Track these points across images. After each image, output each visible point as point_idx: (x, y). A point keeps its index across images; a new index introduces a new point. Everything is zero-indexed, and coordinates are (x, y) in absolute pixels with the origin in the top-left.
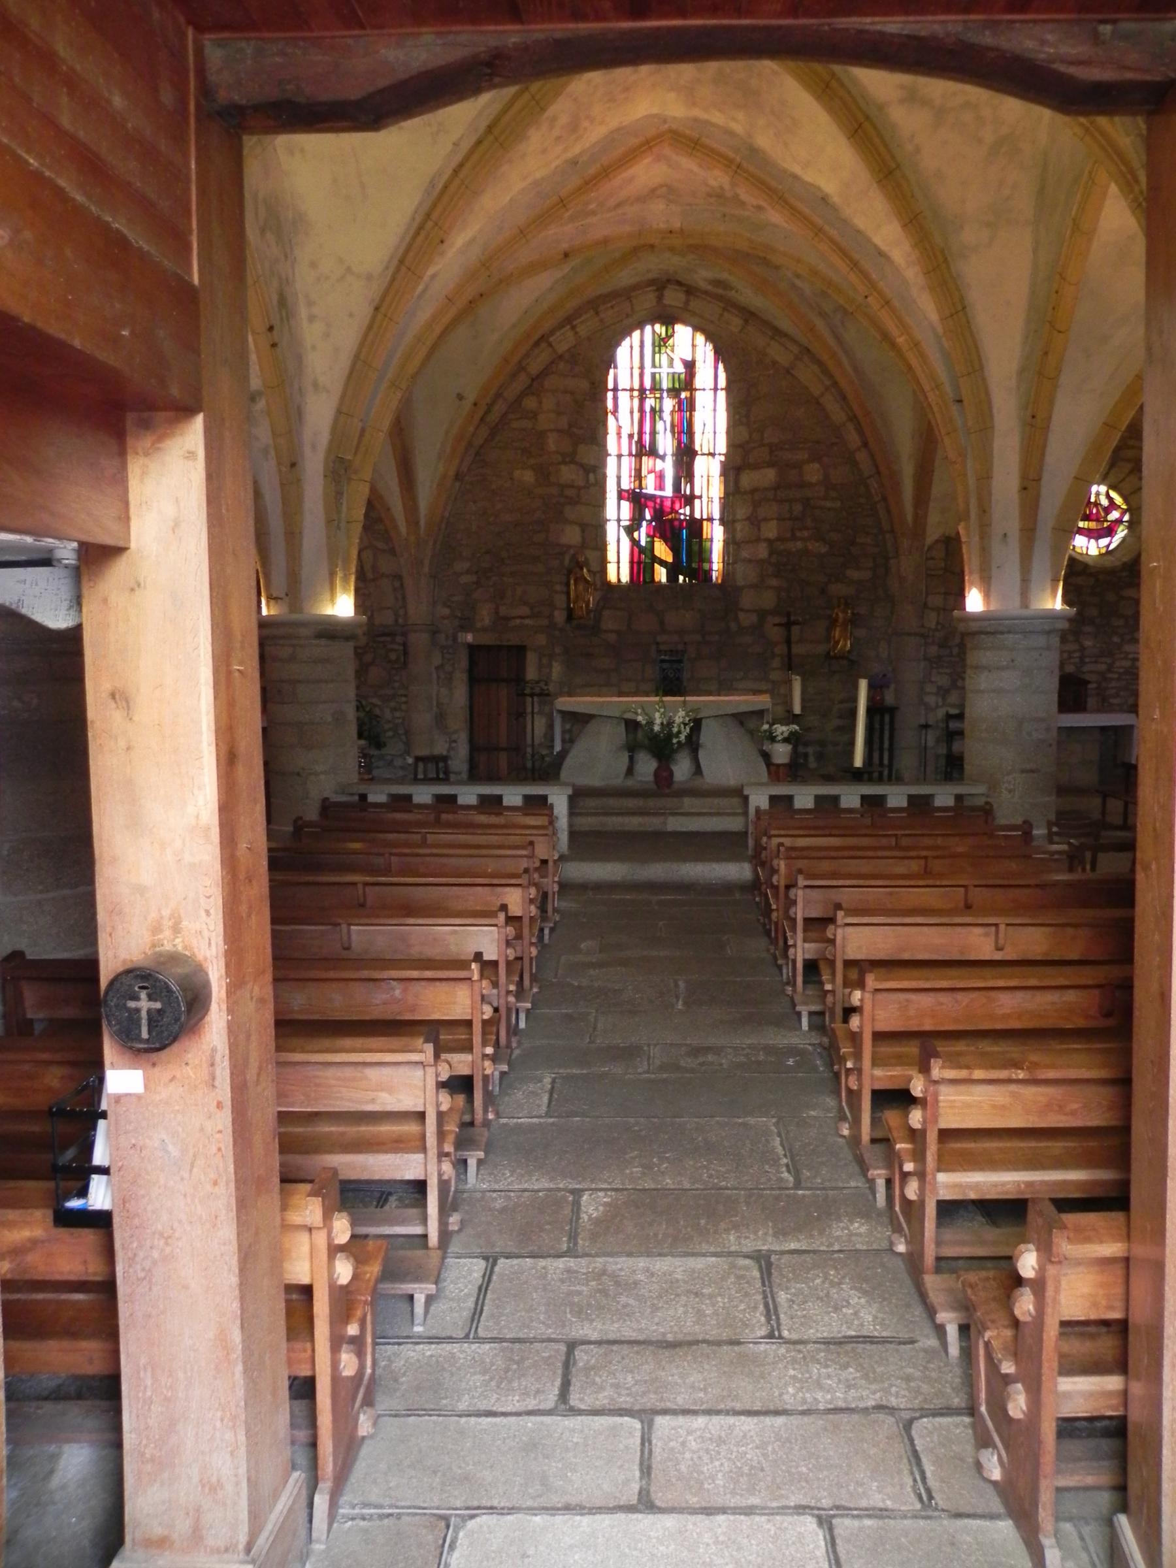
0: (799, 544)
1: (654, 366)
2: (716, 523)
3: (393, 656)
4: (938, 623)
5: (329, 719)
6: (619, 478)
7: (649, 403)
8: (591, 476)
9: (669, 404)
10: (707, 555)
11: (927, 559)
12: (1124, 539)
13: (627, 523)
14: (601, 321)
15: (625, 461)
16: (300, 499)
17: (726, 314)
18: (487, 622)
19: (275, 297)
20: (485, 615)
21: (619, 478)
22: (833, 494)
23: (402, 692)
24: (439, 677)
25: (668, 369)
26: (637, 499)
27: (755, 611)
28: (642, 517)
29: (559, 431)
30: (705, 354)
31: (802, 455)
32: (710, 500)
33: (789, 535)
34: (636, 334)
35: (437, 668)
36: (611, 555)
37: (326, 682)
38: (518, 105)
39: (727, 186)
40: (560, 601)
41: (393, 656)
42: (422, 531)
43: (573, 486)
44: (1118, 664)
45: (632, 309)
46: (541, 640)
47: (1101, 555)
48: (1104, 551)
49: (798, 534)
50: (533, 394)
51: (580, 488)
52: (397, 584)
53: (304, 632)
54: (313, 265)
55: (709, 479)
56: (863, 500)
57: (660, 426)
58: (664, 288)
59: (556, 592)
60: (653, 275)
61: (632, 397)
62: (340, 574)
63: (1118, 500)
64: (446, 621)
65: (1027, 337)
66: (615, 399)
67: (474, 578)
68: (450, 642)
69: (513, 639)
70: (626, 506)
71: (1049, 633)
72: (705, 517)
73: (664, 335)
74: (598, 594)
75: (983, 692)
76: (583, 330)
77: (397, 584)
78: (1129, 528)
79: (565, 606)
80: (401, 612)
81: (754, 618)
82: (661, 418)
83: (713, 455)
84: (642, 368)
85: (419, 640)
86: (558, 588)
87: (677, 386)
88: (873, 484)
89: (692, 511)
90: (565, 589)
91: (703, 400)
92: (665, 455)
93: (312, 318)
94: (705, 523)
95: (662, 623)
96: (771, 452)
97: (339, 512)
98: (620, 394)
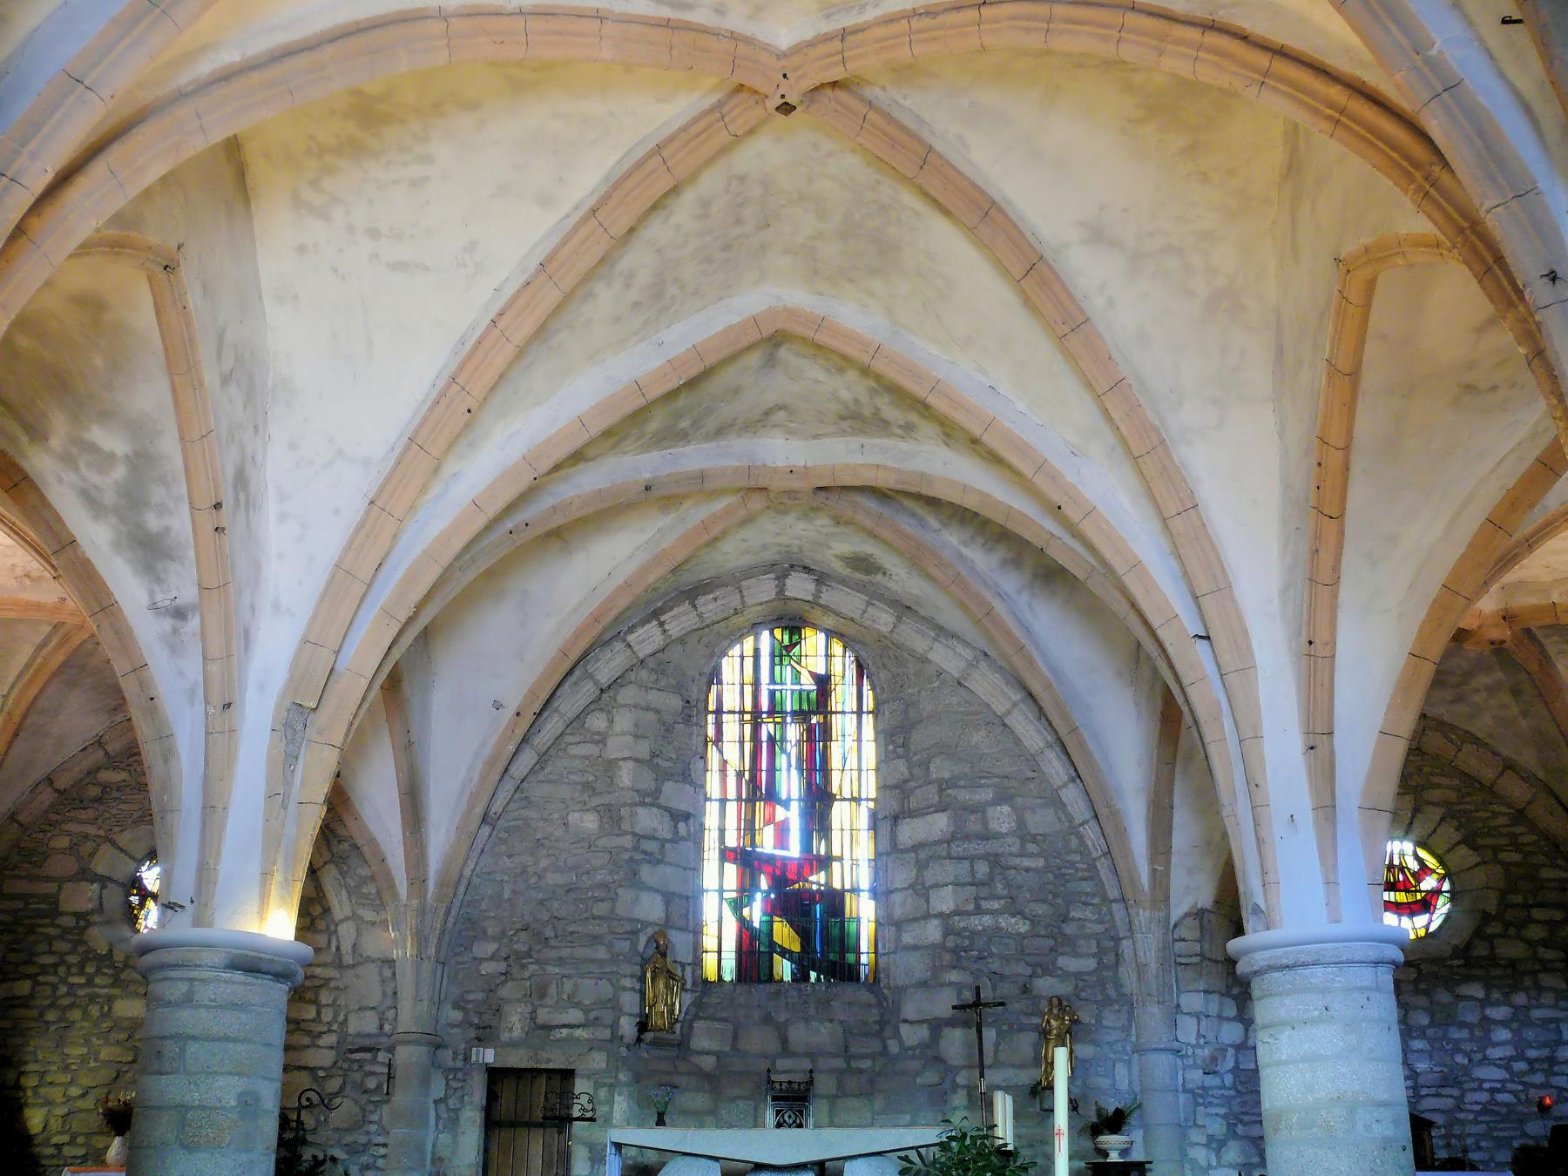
0: (987, 920)
1: (772, 681)
2: (865, 896)
3: (371, 1083)
4: (1199, 1035)
5: (233, 1103)
6: (722, 831)
7: (767, 729)
8: (682, 825)
9: (793, 732)
10: (853, 941)
11: (1175, 940)
12: (1448, 917)
13: (734, 895)
14: (700, 616)
15: (732, 808)
16: (230, 759)
17: (870, 609)
18: (517, 1033)
19: (230, 471)
20: (515, 1022)
21: (722, 831)
22: (1031, 848)
23: (381, 1140)
24: (438, 1117)
25: (793, 685)
26: (746, 860)
27: (923, 1022)
28: (755, 886)
29: (636, 760)
30: (843, 667)
31: (986, 795)
32: (855, 862)
33: (971, 907)
34: (749, 643)
35: (436, 1102)
36: (709, 942)
37: (235, 1040)
38: (583, 233)
39: (864, 398)
40: (630, 1001)
41: (371, 1083)
42: (429, 896)
43: (655, 839)
44: (1470, 1097)
45: (743, 602)
46: (599, 1060)
47: (1419, 939)
48: (1422, 933)
49: (985, 905)
50: (602, 710)
51: (663, 842)
52: (387, 973)
53: (209, 957)
54: (293, 446)
55: (852, 829)
56: (1077, 858)
57: (781, 761)
58: (786, 576)
59: (625, 989)
60: (769, 556)
61: (742, 722)
62: (278, 877)
63: (1431, 862)
64: (455, 1030)
65: (1286, 545)
66: (719, 726)
67: (502, 967)
68: (459, 1064)
69: (555, 1060)
70: (731, 870)
71: (1377, 963)
72: (848, 886)
73: (786, 642)
74: (688, 998)
75: (1285, 1063)
76: (675, 629)
77: (387, 973)
78: (1452, 899)
79: (637, 1011)
80: (390, 1014)
81: (923, 1032)
82: (783, 750)
83: (856, 800)
84: (756, 683)
85: (408, 1056)
86: (627, 982)
87: (805, 707)
88: (1091, 833)
89: (829, 877)
90: (638, 986)
91: (842, 725)
92: (789, 800)
93: (283, 517)
94: (848, 896)
95: (784, 1041)
96: (941, 791)
97: (288, 783)
98: (725, 717)
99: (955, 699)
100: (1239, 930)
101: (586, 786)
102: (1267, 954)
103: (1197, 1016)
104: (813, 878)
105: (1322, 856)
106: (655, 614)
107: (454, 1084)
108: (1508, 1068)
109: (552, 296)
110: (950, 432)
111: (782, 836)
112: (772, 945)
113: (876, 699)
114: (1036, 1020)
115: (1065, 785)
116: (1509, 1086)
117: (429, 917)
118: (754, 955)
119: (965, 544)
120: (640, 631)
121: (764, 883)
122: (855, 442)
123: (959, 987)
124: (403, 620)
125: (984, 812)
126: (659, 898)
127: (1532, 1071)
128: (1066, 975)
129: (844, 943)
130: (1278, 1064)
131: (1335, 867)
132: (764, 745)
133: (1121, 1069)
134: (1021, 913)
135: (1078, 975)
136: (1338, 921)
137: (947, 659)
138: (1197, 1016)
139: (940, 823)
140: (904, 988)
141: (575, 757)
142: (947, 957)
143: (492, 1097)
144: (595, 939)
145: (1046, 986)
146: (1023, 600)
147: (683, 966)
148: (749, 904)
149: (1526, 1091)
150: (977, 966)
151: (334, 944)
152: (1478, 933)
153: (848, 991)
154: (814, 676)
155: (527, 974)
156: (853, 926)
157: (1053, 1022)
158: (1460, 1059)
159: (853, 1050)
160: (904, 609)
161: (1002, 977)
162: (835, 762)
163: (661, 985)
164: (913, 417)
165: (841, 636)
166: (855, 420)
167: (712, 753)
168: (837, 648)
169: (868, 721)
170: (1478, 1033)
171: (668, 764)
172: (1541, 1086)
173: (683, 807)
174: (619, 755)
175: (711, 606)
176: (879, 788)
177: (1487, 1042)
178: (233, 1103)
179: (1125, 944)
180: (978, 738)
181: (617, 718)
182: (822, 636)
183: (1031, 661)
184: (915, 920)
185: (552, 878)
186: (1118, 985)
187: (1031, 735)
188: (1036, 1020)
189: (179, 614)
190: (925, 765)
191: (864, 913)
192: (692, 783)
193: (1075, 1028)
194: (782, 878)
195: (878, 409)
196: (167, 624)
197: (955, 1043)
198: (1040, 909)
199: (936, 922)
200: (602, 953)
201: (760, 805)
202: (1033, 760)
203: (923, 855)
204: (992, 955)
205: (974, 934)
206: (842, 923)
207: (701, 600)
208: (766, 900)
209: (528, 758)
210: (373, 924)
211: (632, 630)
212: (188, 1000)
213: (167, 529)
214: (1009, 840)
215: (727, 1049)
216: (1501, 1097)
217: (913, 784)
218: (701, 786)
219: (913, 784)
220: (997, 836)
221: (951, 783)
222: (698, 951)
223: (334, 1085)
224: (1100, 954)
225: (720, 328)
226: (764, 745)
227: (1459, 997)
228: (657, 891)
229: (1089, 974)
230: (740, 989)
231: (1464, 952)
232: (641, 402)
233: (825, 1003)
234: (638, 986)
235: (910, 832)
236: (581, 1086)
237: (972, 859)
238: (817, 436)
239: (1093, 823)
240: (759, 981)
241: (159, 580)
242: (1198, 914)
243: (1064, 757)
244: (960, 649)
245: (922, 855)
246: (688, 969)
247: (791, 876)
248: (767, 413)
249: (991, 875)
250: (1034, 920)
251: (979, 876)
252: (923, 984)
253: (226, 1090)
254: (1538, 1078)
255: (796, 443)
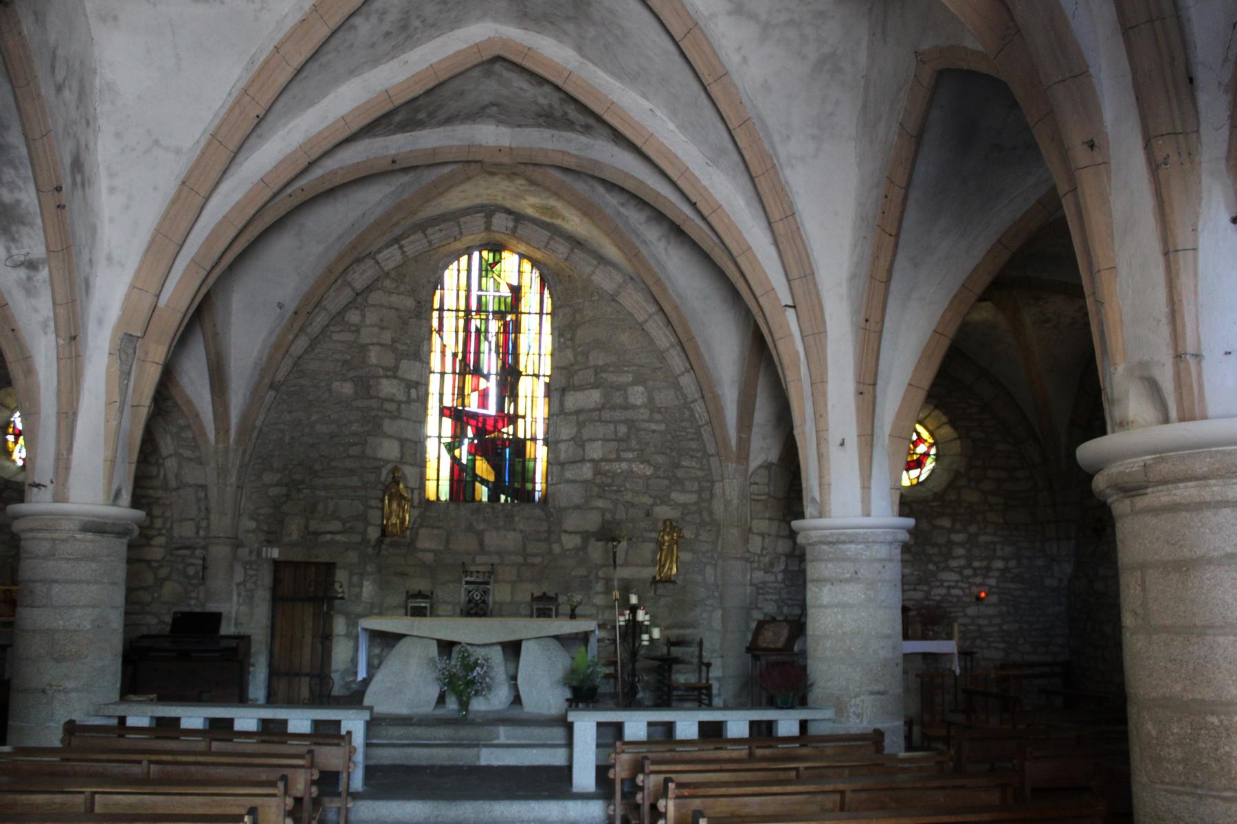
1: (480, 289)
2: (540, 443)
4: (763, 548)
6: (441, 395)
7: (475, 323)
8: (413, 391)
9: (494, 326)
10: (531, 474)
12: (933, 471)
13: (449, 440)
15: (449, 379)
18: (295, 536)
19: (68, 160)
20: (294, 529)
21: (441, 395)
22: (657, 416)
24: (239, 595)
25: (494, 292)
26: (459, 416)
28: (464, 434)
30: (531, 281)
31: (628, 378)
34: (464, 259)
35: (238, 585)
36: (431, 472)
41: (191, 571)
43: (392, 400)
46: (352, 557)
48: (915, 482)
51: (400, 403)
52: (202, 495)
57: (484, 346)
61: (457, 318)
66: (441, 319)
67: (284, 491)
68: (254, 558)
70: (447, 422)
73: (491, 261)
74: (416, 512)
75: (826, 607)
76: (410, 250)
80: (204, 524)
81: (577, 540)
82: (486, 339)
84: (469, 290)
85: (220, 552)
86: (374, 503)
87: (503, 308)
88: (699, 408)
91: (529, 323)
92: (489, 374)
93: (112, 190)
94: (528, 443)
95: (481, 543)
96: (596, 374)
98: (446, 314)
99: (609, 310)
100: (801, 515)
101: (345, 362)
102: (820, 533)
103: (763, 535)
104: (505, 430)
105: (862, 474)
106: (396, 240)
107: (251, 572)
108: (960, 573)
109: (323, 32)
110: (618, 137)
111: (482, 398)
112: (475, 477)
113: (553, 304)
114: (654, 535)
115: (682, 374)
116: (960, 584)
117: (231, 455)
118: (462, 479)
119: (622, 205)
120: (386, 252)
121: (470, 433)
122: (547, 133)
123: (603, 511)
124: (208, 268)
125: (625, 391)
126: (396, 444)
127: (975, 575)
128: (676, 505)
129: (526, 475)
130: (821, 606)
131: (870, 476)
132: (473, 335)
133: (709, 571)
134: (648, 462)
135: (684, 505)
136: (868, 515)
137: (605, 281)
138: (763, 535)
139: (595, 396)
140: (566, 509)
141: (337, 341)
142: (596, 490)
143: (277, 581)
144: (351, 472)
145: (663, 512)
146: (661, 245)
147: (412, 490)
148: (460, 447)
149: (969, 588)
150: (615, 497)
151: (162, 473)
152: (951, 485)
153: (527, 509)
154: (511, 287)
155: (301, 496)
156: (532, 464)
157: (666, 538)
158: (931, 567)
159: (529, 550)
160: (576, 243)
161: (633, 505)
162: (523, 349)
163: (395, 505)
164: (591, 121)
165: (530, 259)
166: (548, 119)
167: (435, 338)
168: (527, 265)
169: (547, 320)
170: (944, 550)
171: (404, 347)
172: (980, 585)
173: (414, 377)
174: (368, 341)
175: (438, 235)
176: (553, 368)
177: (948, 556)
178: (88, 627)
179: (717, 485)
180: (624, 338)
181: (368, 314)
182: (516, 257)
183: (664, 290)
184: (573, 462)
185: (320, 428)
186: (711, 513)
187: (662, 338)
188: (654, 535)
189: (32, 265)
190: (586, 355)
191: (539, 454)
192: (421, 361)
193: (681, 541)
194: (483, 426)
195: (566, 113)
196: (22, 273)
197: (596, 551)
198: (660, 459)
199: (589, 465)
200: (355, 481)
201: (468, 378)
202: (661, 355)
203: (582, 417)
204: (626, 489)
205: (615, 475)
206: (524, 461)
207: (429, 231)
208: (471, 445)
209: (302, 343)
210: (190, 459)
211: (379, 251)
212: (51, 555)
213: (18, 202)
214: (642, 410)
215: (442, 548)
216: (954, 592)
217: (577, 367)
218: (427, 362)
219: (577, 367)
220: (634, 407)
221: (603, 369)
222: (422, 478)
223: (163, 572)
224: (700, 491)
225: (450, 52)
226: (473, 335)
227: (935, 527)
228: (396, 438)
229: (692, 504)
230: (452, 506)
231: (940, 497)
232: (389, 107)
233: (510, 517)
234: (380, 505)
235: (573, 401)
236: (341, 576)
237: (616, 423)
238: (519, 126)
239: (700, 401)
240: (465, 501)
241: (14, 240)
242: (767, 466)
243: (682, 354)
244: (614, 272)
245: (581, 418)
246: (416, 492)
247: (489, 428)
248: (484, 108)
249: (628, 436)
250: (656, 467)
251: (620, 435)
252: (577, 507)
253: (82, 619)
254: (979, 580)
255: (504, 130)
